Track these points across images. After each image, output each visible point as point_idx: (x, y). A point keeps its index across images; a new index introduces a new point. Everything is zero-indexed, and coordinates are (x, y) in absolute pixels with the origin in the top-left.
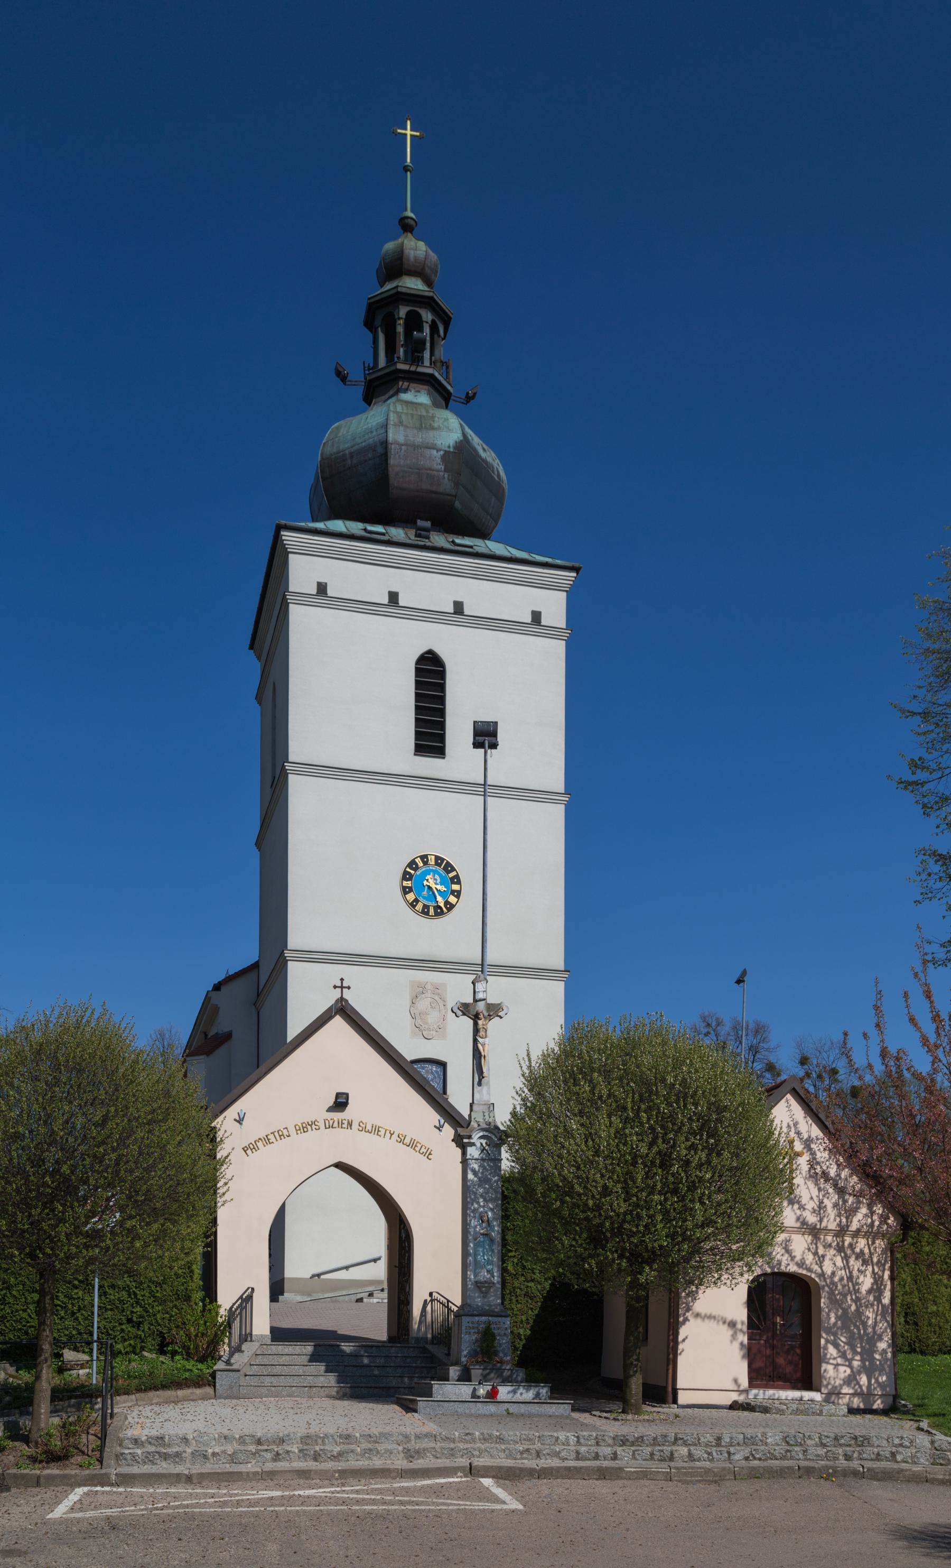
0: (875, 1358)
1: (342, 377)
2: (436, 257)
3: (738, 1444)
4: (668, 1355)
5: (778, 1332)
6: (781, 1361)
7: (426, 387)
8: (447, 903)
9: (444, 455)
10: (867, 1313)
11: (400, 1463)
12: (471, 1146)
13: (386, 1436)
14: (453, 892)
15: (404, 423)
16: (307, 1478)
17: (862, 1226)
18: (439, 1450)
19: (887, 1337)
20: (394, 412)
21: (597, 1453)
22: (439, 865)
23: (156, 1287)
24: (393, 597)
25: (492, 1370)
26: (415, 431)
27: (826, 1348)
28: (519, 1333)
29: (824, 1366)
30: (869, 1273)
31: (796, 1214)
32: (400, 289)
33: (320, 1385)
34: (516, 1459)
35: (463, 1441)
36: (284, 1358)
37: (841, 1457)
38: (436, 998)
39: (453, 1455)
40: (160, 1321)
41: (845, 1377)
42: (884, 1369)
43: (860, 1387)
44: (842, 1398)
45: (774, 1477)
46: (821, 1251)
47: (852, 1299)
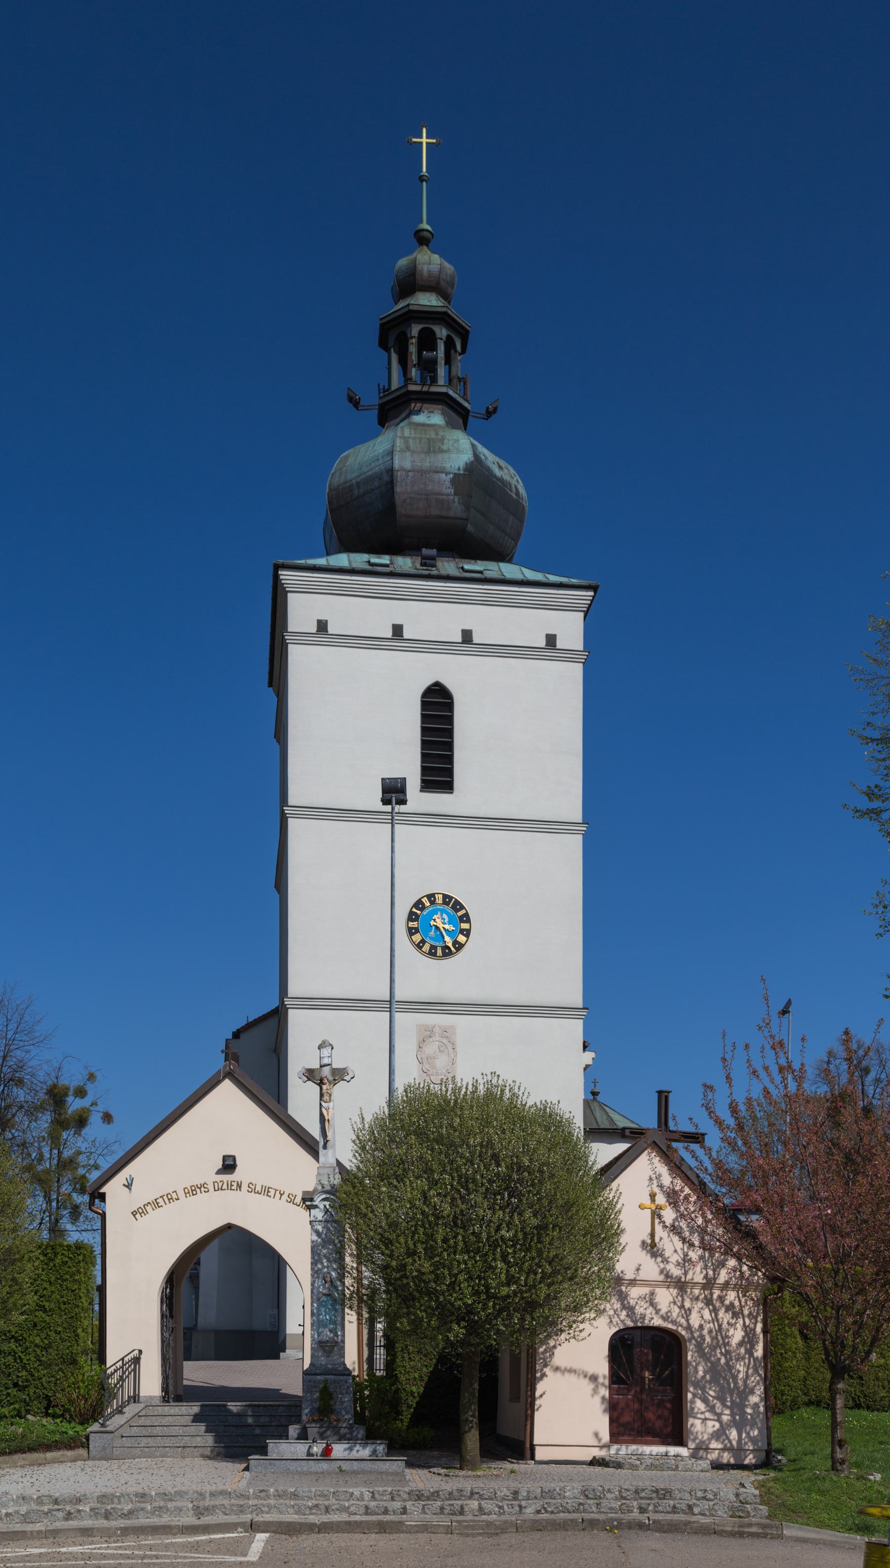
0: (746, 1413)
1: (354, 402)
2: (452, 269)
3: (536, 1498)
4: (527, 1410)
5: (647, 1387)
6: (650, 1415)
7: (440, 407)
8: (455, 943)
9: (454, 478)
10: (738, 1366)
11: (189, 1520)
12: (314, 1208)
13: (180, 1494)
14: (462, 931)
15: (412, 448)
16: (89, 1536)
17: (731, 1278)
18: (228, 1507)
19: (760, 1390)
20: (400, 437)
21: (386, 1507)
22: (447, 904)
23: (42, 1351)
24: (398, 630)
25: (328, 1428)
26: (423, 456)
27: (693, 1402)
28: (411, 1391)
29: (691, 1421)
30: (739, 1326)
31: (659, 1266)
32: (411, 307)
33: (194, 1445)
34: (304, 1514)
35: (257, 1497)
36: (167, 1419)
37: (635, 1510)
38: (445, 1041)
39: (242, 1512)
40: (45, 1385)
41: (714, 1432)
42: (756, 1423)
43: (730, 1441)
44: (711, 1453)
45: (556, 1529)
46: (687, 1304)
47: (721, 1353)
